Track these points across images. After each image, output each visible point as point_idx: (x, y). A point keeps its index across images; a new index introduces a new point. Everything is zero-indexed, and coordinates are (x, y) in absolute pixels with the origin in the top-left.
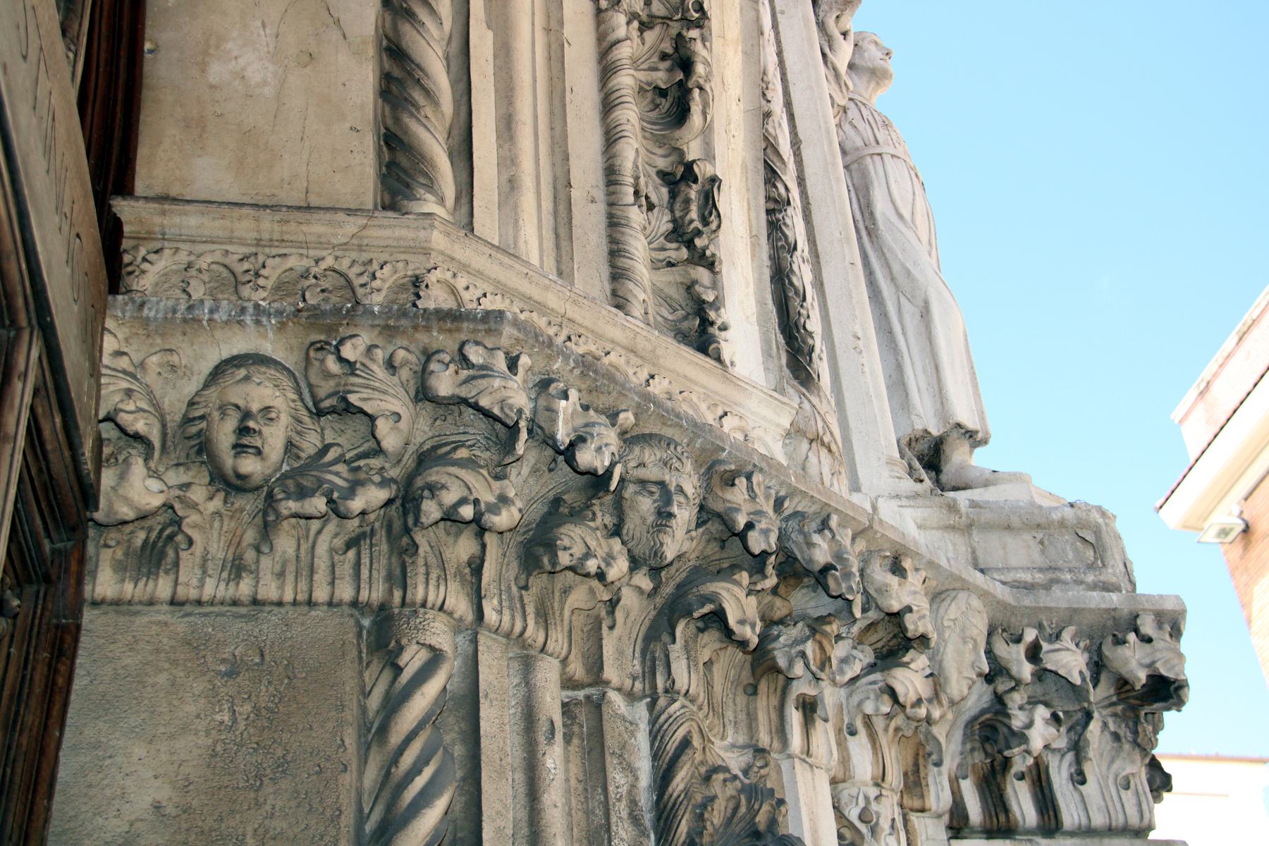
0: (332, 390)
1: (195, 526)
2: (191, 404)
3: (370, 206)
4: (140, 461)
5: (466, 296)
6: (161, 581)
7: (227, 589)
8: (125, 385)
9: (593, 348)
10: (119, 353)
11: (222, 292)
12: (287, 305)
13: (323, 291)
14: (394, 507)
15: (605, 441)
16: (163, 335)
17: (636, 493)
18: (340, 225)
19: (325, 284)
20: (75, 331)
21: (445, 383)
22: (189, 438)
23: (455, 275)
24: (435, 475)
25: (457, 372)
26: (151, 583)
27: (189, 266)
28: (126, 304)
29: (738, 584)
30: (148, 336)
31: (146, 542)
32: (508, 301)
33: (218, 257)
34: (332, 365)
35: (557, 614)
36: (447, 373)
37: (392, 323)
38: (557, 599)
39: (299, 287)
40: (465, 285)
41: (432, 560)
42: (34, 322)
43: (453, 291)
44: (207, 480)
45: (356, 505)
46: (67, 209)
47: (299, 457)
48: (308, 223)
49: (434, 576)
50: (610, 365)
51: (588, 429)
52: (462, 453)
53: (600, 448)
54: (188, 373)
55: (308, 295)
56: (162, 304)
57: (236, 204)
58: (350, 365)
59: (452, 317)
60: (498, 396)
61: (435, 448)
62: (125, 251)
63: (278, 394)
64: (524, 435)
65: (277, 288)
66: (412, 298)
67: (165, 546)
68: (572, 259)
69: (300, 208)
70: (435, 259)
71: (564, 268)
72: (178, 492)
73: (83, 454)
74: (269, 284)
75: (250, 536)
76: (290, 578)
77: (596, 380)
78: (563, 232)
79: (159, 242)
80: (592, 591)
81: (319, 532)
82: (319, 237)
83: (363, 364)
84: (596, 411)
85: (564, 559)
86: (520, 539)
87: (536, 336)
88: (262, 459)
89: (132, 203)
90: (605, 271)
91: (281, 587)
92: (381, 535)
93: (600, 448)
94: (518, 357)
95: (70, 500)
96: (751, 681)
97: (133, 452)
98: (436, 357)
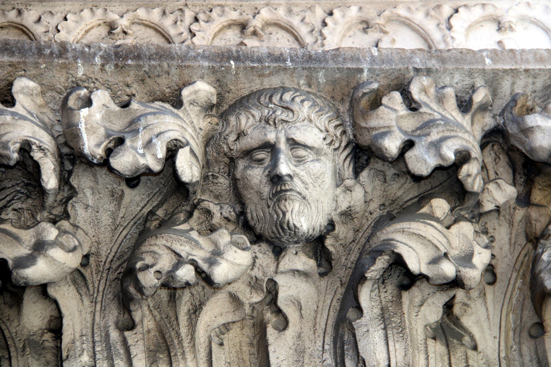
15: (157, 131)
17: (246, 168)
23: (20, 12)
24: (148, 225)
29: (431, 217)
35: (186, 344)
53: (150, 141)
77: (139, 67)
93: (150, 141)
96: (536, 320)
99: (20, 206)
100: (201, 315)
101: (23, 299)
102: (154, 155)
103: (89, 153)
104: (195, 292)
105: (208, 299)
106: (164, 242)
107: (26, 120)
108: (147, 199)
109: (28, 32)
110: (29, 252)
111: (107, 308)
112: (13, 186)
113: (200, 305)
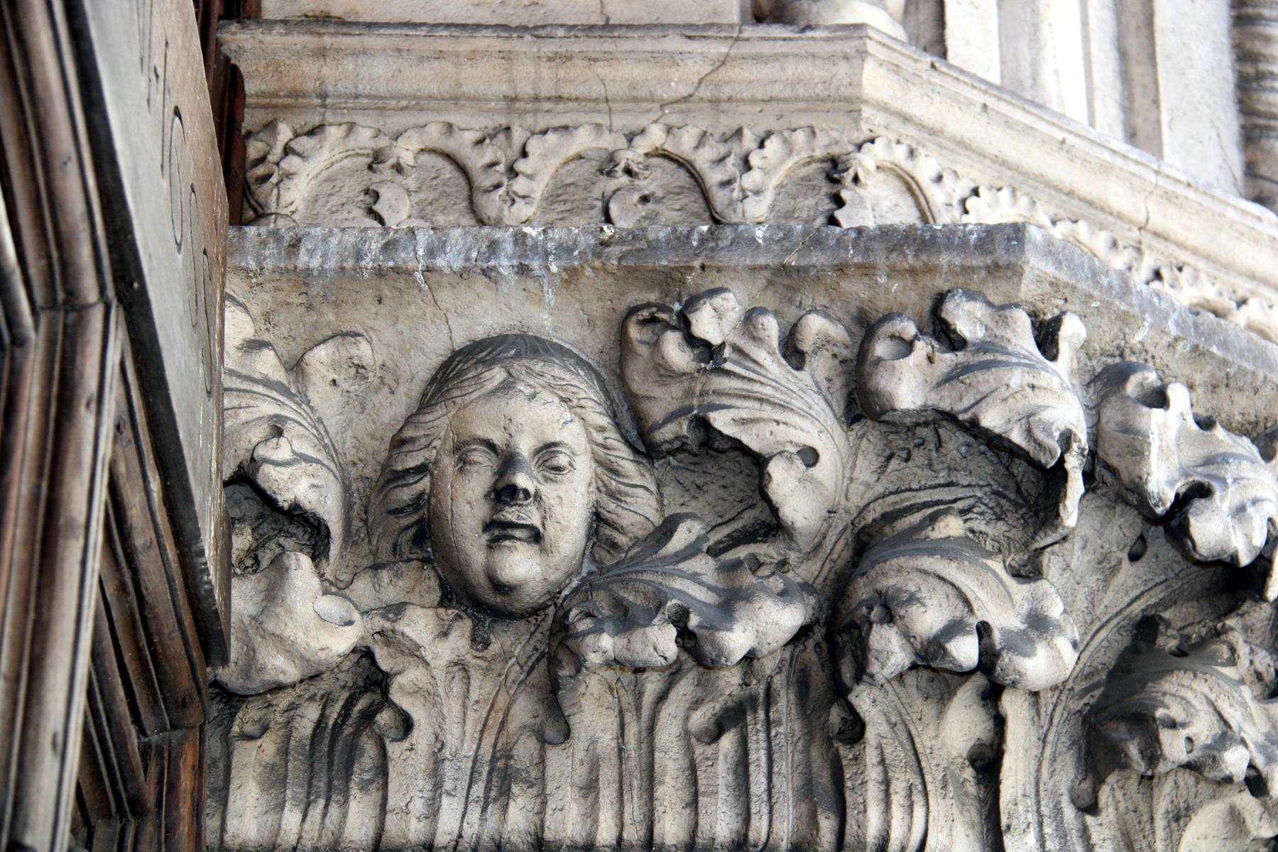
0: (676, 405)
1: (416, 691)
2: (399, 443)
3: (735, 17)
4: (305, 560)
5: (936, 196)
6: (354, 806)
7: (483, 819)
8: (269, 409)
9: (1209, 292)
10: (253, 345)
11: (444, 210)
12: (580, 230)
13: (645, 199)
14: (810, 644)
15: (1252, 493)
16: (336, 305)
18: (674, 59)
19: (648, 185)
20: (180, 306)
21: (908, 384)
22: (396, 512)
23: (912, 153)
24: (895, 574)
25: (930, 359)
26: (334, 810)
27: (376, 159)
28: (264, 244)
30: (310, 307)
31: (320, 724)
32: (1024, 201)
33: (433, 134)
34: (675, 352)
36: (911, 360)
37: (792, 260)
38: (1160, 833)
39: (597, 193)
40: (934, 174)
41: (898, 754)
42: (111, 292)
43: (910, 187)
44: (436, 596)
45: (737, 640)
46: (157, 61)
47: (614, 546)
48: (609, 58)
49: (898, 787)
50: (1250, 327)
51: (1211, 469)
52: (952, 526)
54: (389, 379)
55: (614, 210)
56: (334, 241)
57: (464, 26)
58: (708, 352)
59: (920, 241)
60: (1020, 405)
61: (890, 517)
62: (249, 134)
63: (568, 416)
64: (1076, 486)
65: (554, 197)
66: (827, 205)
67: (357, 733)
68: (1156, 102)
69: (592, 27)
70: (871, 119)
71: (1139, 122)
72: (379, 623)
73: (202, 553)
74: (538, 189)
75: (524, 710)
76: (607, 795)
78: (1134, 44)
79: (315, 111)
80: (1235, 818)
81: (662, 698)
82: (633, 87)
83: (738, 350)
84: (1229, 428)
85: (1174, 747)
86: (1076, 705)
87: (1095, 274)
88: (544, 551)
89: (258, 33)
90: (1230, 123)
91: (592, 814)
92: (785, 703)
94: (1057, 321)
95: (177, 646)
97: (288, 543)
98: (888, 328)
99: (983, 528)
100: (1187, 829)
101: (955, 694)
102: (1248, 537)
103: (1156, 491)
104: (1182, 784)
105: (1201, 804)
106: (1206, 690)
107: (989, 368)
108: (1142, 588)
109: (918, 192)
110: (1023, 627)
111: (1059, 759)
112: (969, 486)
113: (1187, 809)
